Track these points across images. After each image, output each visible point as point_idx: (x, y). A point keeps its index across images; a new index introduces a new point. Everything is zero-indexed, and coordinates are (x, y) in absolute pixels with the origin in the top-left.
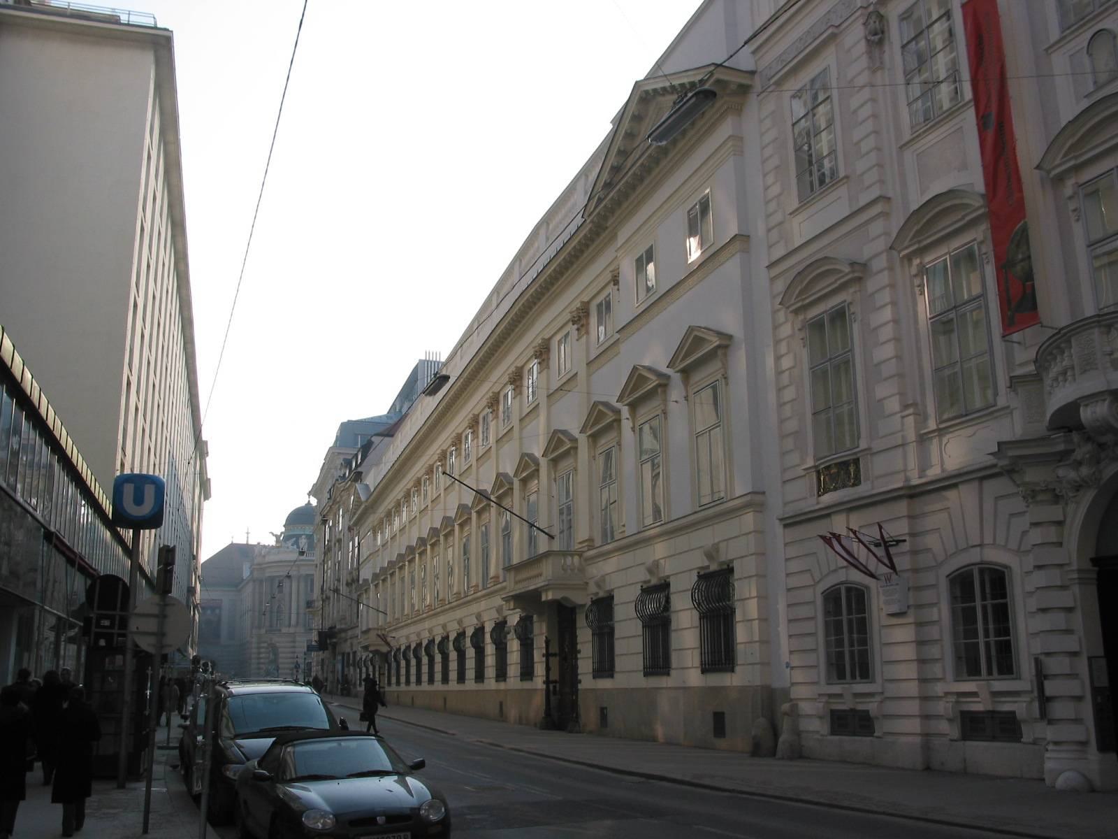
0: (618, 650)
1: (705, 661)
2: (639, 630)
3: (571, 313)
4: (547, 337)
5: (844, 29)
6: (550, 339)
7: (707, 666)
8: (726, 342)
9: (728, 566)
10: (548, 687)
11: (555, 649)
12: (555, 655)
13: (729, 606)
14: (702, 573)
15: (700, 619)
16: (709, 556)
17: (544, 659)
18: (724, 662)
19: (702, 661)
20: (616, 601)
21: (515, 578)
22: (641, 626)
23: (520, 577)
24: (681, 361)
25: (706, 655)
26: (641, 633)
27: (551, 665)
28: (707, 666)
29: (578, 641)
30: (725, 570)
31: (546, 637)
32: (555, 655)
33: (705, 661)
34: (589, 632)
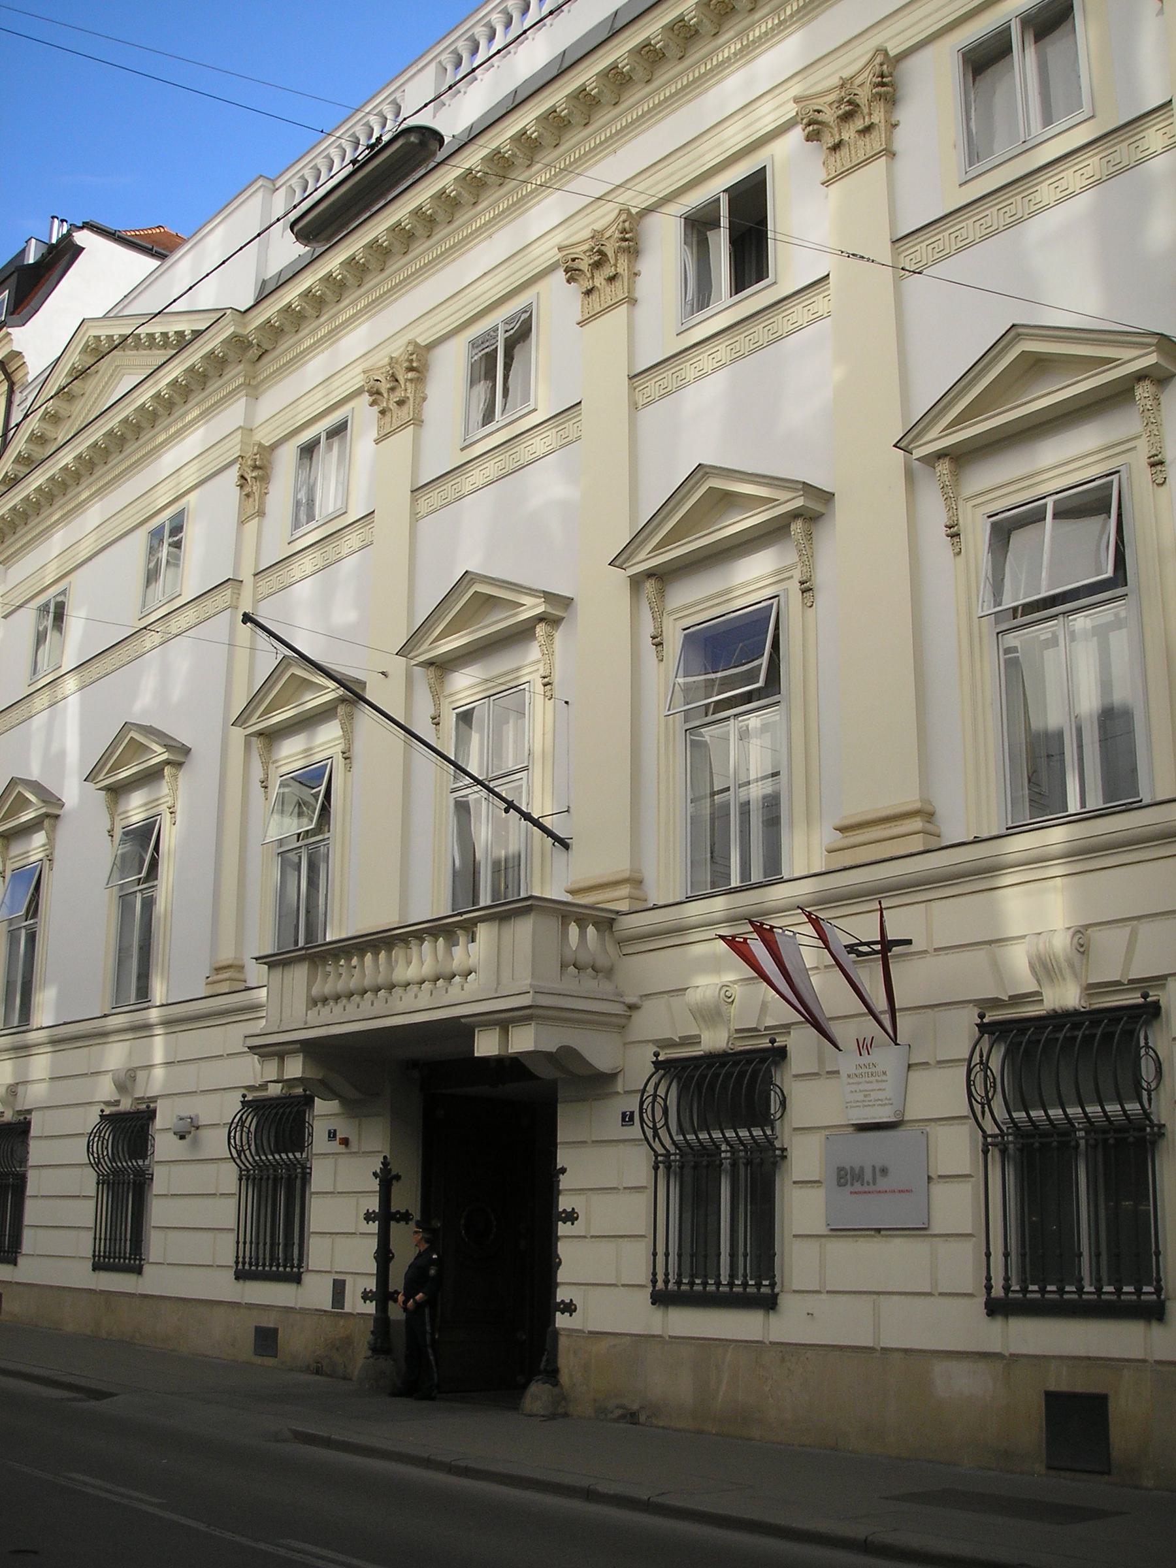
0: (29, 1217)
1: (244, 1258)
2: (90, 1188)
3: (797, 100)
4: (422, 341)
5: (262, 381)
6: (274, 447)
7: (247, 1267)
8: (180, 755)
9: (148, 1107)
10: (382, 1308)
11: (407, 1198)
12: (405, 1217)
13: (299, 1162)
14: (107, 1112)
15: (985, 1152)
16: (121, 1087)
17: (374, 1227)
18: (296, 1262)
19: (237, 1257)
20: (33, 1132)
21: (309, 986)
22: (95, 1181)
23: (327, 985)
24: (951, 425)
25: (248, 1245)
26: (94, 1194)
27: (393, 1246)
28: (247, 1267)
29: (561, 1188)
30: (143, 1112)
31: (385, 1157)
32: (405, 1217)
33: (244, 1258)
34: (636, 1165)
